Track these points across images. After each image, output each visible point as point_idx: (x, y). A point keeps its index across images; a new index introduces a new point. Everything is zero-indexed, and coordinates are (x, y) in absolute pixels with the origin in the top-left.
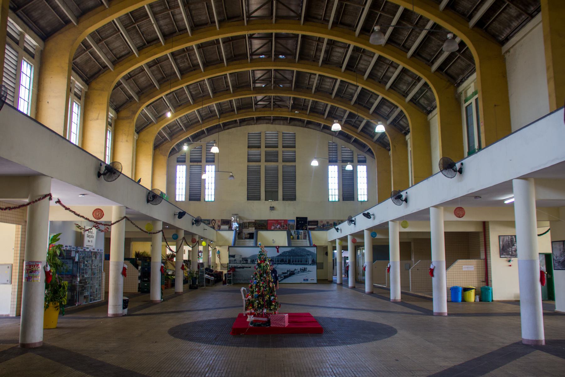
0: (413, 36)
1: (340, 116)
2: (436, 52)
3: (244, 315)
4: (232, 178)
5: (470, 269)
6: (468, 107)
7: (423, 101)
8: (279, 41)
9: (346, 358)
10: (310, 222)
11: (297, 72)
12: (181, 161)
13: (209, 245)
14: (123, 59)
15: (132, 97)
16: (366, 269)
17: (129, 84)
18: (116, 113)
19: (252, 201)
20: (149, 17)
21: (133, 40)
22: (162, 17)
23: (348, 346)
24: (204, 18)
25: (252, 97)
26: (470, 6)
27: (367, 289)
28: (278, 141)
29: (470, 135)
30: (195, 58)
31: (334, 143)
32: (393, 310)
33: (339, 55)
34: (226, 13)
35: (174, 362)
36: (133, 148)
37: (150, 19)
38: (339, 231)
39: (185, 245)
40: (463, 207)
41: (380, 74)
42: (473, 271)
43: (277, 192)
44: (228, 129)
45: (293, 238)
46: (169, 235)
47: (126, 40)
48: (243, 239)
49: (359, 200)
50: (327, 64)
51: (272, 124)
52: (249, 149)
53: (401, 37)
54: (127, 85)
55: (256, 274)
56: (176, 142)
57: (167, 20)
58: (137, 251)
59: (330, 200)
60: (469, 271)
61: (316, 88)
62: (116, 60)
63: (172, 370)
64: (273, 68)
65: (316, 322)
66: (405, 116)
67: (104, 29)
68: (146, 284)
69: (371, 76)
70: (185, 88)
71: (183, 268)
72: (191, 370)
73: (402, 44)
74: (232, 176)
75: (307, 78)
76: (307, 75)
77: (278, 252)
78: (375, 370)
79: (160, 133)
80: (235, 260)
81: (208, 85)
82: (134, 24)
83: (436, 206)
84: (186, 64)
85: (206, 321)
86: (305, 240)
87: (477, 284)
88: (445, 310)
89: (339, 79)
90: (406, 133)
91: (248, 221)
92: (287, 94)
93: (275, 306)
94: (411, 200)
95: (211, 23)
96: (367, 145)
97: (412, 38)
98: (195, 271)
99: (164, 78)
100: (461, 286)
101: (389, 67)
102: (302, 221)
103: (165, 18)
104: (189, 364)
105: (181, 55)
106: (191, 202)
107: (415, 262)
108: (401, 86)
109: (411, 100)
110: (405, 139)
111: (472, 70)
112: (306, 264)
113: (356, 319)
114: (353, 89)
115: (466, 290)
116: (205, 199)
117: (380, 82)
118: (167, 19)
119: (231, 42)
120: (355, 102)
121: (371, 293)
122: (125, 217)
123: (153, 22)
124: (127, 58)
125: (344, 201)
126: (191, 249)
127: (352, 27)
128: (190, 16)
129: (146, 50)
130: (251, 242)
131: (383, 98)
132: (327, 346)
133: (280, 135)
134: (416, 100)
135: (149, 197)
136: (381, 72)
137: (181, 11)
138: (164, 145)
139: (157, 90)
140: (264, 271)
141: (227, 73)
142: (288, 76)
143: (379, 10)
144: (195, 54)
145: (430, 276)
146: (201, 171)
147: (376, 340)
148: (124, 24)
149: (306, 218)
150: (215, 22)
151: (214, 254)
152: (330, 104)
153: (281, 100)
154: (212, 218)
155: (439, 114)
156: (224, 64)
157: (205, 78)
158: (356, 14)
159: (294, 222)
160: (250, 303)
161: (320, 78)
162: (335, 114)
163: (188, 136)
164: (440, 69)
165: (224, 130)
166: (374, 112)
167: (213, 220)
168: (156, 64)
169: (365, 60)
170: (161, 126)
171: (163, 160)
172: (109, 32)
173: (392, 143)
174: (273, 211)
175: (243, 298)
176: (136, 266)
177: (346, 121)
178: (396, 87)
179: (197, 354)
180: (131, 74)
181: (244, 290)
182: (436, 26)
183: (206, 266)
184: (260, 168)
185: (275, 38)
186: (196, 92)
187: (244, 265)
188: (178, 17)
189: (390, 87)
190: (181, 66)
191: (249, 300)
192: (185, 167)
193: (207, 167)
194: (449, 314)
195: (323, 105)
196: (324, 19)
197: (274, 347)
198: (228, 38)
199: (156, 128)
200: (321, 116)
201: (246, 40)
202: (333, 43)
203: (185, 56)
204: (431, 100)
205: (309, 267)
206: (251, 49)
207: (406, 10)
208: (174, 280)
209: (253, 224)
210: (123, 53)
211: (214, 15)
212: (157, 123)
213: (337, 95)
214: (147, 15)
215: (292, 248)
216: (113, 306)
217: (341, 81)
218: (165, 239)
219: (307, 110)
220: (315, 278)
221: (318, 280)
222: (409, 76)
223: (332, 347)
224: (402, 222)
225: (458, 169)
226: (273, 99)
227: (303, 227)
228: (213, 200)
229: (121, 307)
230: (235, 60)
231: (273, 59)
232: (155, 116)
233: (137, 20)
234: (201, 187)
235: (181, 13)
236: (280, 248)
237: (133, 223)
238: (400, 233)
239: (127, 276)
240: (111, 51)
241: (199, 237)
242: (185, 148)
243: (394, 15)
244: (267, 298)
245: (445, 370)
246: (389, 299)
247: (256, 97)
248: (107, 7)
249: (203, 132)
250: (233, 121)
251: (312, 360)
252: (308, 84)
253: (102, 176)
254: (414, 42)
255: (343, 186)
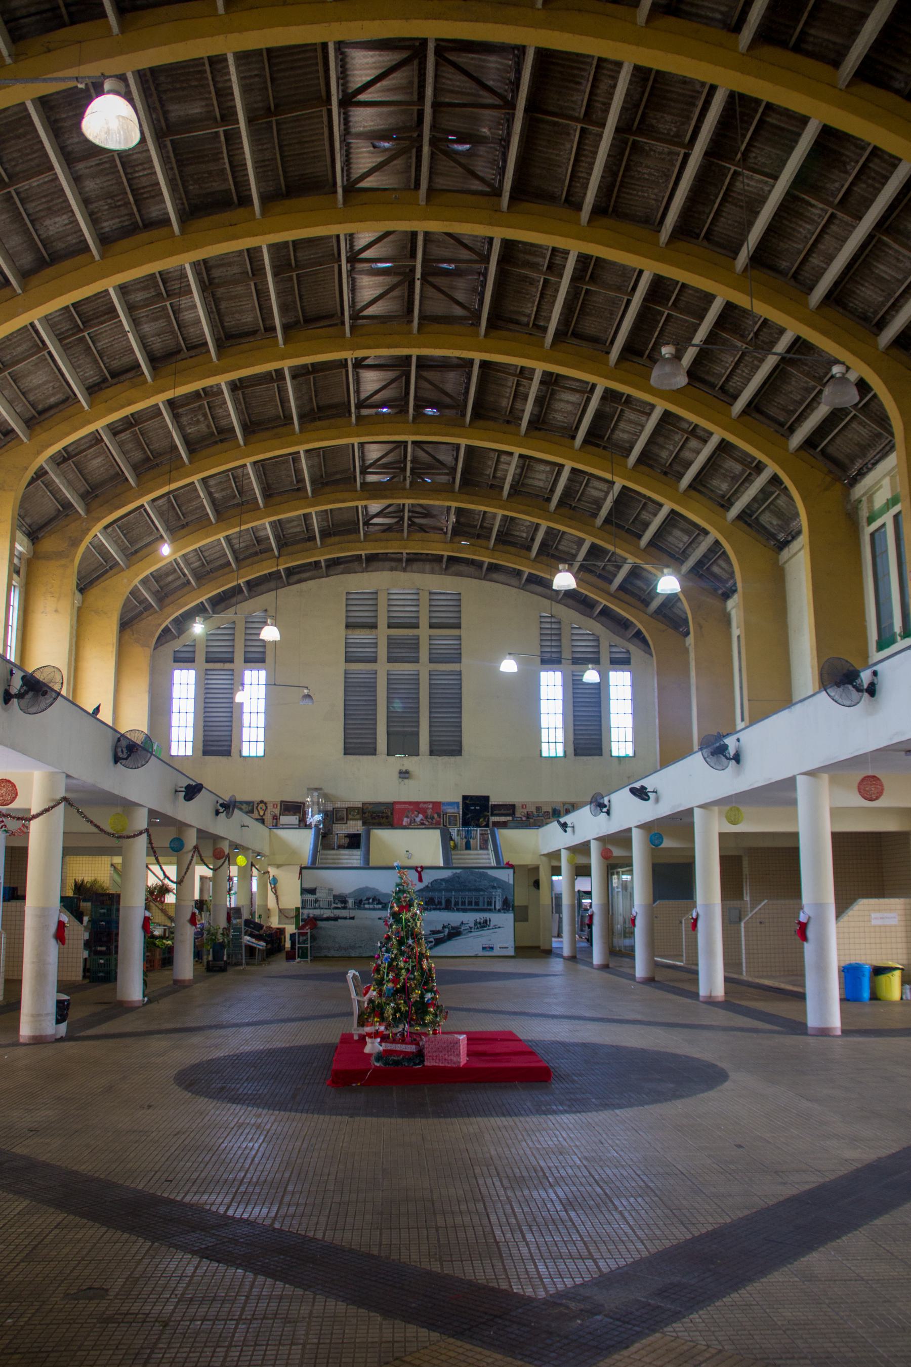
0: (746, 366)
1: (568, 553)
2: (800, 403)
3: (356, 1038)
4: (307, 702)
5: (887, 922)
6: (877, 534)
7: (767, 519)
8: (425, 374)
9: (617, 1142)
10: (496, 807)
11: (469, 448)
12: (184, 659)
13: (252, 865)
14: (52, 416)
15: (71, 505)
16: (637, 922)
17: (64, 475)
18: (31, 544)
19: (357, 757)
20: (119, 317)
21: (78, 370)
22: (147, 316)
23: (617, 1111)
24: (248, 320)
25: (357, 507)
26: (881, 299)
27: (640, 970)
28: (418, 611)
29: (882, 600)
30: (225, 413)
31: (552, 616)
32: (709, 1023)
33: (570, 408)
34: (302, 307)
35: (203, 1155)
36: (72, 627)
37: (120, 321)
38: (568, 829)
39: (197, 864)
40: (878, 776)
41: (665, 455)
42: (896, 926)
43: (417, 734)
44: (299, 581)
45: (455, 847)
46: (163, 840)
47: (60, 370)
48: (333, 849)
49: (615, 753)
50: (540, 429)
51: (404, 570)
52: (350, 632)
53: (718, 369)
54: (58, 476)
55: (389, 938)
56: (173, 613)
57: (162, 323)
58: (79, 879)
59: (545, 753)
60: (885, 926)
61: (512, 487)
62: (34, 417)
63: (203, 1175)
64: (410, 438)
65: (532, 1053)
66: (724, 553)
67: (8, 343)
68: (102, 961)
69: (645, 458)
70: (197, 484)
71: (193, 921)
72: (249, 1176)
73: (719, 386)
74: (308, 696)
75: (490, 463)
76: (492, 454)
77: (420, 880)
78: (693, 1172)
79: (134, 593)
80: (316, 901)
81: (253, 478)
82: (82, 331)
83: (811, 773)
84: (203, 427)
85: (262, 1052)
86: (485, 852)
87: (905, 957)
88: (836, 1022)
89: (569, 465)
90: (727, 596)
91: (347, 806)
92: (443, 500)
93: (436, 1015)
94: (748, 758)
95: (266, 330)
96: (632, 623)
97: (743, 371)
98: (222, 927)
99: (148, 459)
100: (869, 962)
101: (687, 439)
102: (478, 805)
103: (156, 319)
104: (241, 1160)
105: (192, 406)
106: (206, 757)
107: (755, 902)
108: (715, 482)
109: (739, 517)
110: (725, 608)
111: (884, 448)
112: (490, 910)
113: (624, 1044)
114: (601, 490)
115: (879, 971)
116: (240, 751)
117: (665, 473)
118: (160, 321)
119: (312, 377)
120: (607, 521)
121: (650, 981)
122: (65, 799)
123: (127, 328)
124: (60, 411)
125: (577, 758)
126: (209, 873)
127: (602, 344)
128: (215, 314)
129: (109, 392)
130: (354, 857)
131: (673, 511)
132: (566, 1112)
133: (425, 598)
134: (751, 516)
135: (119, 750)
136: (667, 449)
137: (193, 301)
138: (144, 621)
139: (132, 487)
140: (407, 932)
141: (301, 449)
142: (446, 457)
143: (665, 305)
144: (226, 403)
145: (797, 938)
146: (232, 684)
147: (682, 1097)
148: (58, 332)
149: (487, 798)
150: (274, 329)
151: (262, 886)
152: (544, 524)
153: (427, 513)
154: (257, 798)
155: (807, 549)
156: (294, 429)
157: (248, 461)
158: (611, 314)
159: (458, 807)
160: (374, 1008)
161: (521, 461)
162: (556, 548)
163: (203, 599)
164: (810, 443)
165: (289, 584)
166: (651, 543)
167: (262, 802)
168: (131, 425)
169: (630, 421)
170: (137, 575)
171: (140, 657)
172: (19, 349)
173: (693, 618)
174: (406, 781)
175: (353, 995)
176: (79, 916)
177: (581, 565)
178: (704, 486)
179: (256, 1136)
180: (70, 449)
181: (354, 977)
182: (800, 345)
183: (246, 915)
184: (376, 678)
185: (418, 366)
186: (224, 493)
187: (338, 913)
188: (186, 317)
189: (691, 486)
190: (189, 431)
191: (371, 1001)
192: (192, 673)
193: (247, 674)
194: (845, 1032)
195: (527, 527)
196: (534, 324)
197: (440, 1117)
198: (305, 366)
199: (125, 580)
200: (524, 552)
201: (347, 371)
202: (556, 380)
203: (201, 407)
204: (788, 517)
205: (496, 918)
206: (358, 391)
207: (729, 307)
208: (170, 950)
209: (358, 813)
210: (52, 400)
211: (272, 313)
212: (128, 567)
213: (561, 503)
214: (114, 310)
215: (454, 871)
216: (32, 1016)
217: (573, 470)
218: (154, 852)
219: (488, 538)
220: (511, 944)
221: (517, 948)
222: (736, 459)
223: (578, 1114)
224: (727, 808)
225: (865, 686)
226: (409, 511)
227: (478, 820)
228: (261, 753)
229: (53, 1018)
230: (320, 419)
231: (411, 417)
232: (123, 550)
233: (87, 322)
234: (231, 721)
235: (195, 306)
236: (425, 871)
237: (81, 813)
238: (721, 835)
239: (66, 946)
240: (23, 394)
241: (230, 846)
242: (198, 628)
243: (702, 318)
244: (415, 995)
245: (858, 1170)
246: (695, 995)
247: (366, 507)
248: (19, 291)
249: (237, 590)
250: (310, 563)
251: (538, 1149)
252: (494, 477)
253: (15, 700)
254: (749, 380)
255: (574, 721)
